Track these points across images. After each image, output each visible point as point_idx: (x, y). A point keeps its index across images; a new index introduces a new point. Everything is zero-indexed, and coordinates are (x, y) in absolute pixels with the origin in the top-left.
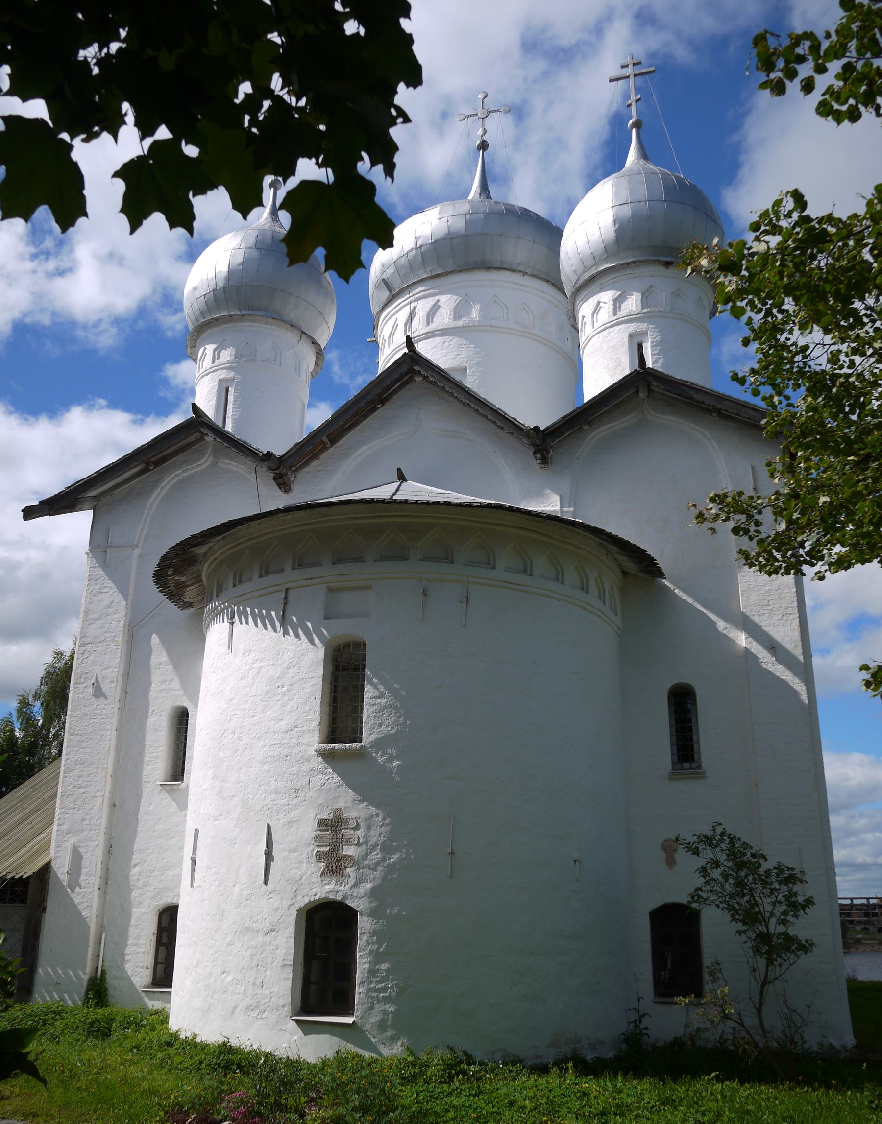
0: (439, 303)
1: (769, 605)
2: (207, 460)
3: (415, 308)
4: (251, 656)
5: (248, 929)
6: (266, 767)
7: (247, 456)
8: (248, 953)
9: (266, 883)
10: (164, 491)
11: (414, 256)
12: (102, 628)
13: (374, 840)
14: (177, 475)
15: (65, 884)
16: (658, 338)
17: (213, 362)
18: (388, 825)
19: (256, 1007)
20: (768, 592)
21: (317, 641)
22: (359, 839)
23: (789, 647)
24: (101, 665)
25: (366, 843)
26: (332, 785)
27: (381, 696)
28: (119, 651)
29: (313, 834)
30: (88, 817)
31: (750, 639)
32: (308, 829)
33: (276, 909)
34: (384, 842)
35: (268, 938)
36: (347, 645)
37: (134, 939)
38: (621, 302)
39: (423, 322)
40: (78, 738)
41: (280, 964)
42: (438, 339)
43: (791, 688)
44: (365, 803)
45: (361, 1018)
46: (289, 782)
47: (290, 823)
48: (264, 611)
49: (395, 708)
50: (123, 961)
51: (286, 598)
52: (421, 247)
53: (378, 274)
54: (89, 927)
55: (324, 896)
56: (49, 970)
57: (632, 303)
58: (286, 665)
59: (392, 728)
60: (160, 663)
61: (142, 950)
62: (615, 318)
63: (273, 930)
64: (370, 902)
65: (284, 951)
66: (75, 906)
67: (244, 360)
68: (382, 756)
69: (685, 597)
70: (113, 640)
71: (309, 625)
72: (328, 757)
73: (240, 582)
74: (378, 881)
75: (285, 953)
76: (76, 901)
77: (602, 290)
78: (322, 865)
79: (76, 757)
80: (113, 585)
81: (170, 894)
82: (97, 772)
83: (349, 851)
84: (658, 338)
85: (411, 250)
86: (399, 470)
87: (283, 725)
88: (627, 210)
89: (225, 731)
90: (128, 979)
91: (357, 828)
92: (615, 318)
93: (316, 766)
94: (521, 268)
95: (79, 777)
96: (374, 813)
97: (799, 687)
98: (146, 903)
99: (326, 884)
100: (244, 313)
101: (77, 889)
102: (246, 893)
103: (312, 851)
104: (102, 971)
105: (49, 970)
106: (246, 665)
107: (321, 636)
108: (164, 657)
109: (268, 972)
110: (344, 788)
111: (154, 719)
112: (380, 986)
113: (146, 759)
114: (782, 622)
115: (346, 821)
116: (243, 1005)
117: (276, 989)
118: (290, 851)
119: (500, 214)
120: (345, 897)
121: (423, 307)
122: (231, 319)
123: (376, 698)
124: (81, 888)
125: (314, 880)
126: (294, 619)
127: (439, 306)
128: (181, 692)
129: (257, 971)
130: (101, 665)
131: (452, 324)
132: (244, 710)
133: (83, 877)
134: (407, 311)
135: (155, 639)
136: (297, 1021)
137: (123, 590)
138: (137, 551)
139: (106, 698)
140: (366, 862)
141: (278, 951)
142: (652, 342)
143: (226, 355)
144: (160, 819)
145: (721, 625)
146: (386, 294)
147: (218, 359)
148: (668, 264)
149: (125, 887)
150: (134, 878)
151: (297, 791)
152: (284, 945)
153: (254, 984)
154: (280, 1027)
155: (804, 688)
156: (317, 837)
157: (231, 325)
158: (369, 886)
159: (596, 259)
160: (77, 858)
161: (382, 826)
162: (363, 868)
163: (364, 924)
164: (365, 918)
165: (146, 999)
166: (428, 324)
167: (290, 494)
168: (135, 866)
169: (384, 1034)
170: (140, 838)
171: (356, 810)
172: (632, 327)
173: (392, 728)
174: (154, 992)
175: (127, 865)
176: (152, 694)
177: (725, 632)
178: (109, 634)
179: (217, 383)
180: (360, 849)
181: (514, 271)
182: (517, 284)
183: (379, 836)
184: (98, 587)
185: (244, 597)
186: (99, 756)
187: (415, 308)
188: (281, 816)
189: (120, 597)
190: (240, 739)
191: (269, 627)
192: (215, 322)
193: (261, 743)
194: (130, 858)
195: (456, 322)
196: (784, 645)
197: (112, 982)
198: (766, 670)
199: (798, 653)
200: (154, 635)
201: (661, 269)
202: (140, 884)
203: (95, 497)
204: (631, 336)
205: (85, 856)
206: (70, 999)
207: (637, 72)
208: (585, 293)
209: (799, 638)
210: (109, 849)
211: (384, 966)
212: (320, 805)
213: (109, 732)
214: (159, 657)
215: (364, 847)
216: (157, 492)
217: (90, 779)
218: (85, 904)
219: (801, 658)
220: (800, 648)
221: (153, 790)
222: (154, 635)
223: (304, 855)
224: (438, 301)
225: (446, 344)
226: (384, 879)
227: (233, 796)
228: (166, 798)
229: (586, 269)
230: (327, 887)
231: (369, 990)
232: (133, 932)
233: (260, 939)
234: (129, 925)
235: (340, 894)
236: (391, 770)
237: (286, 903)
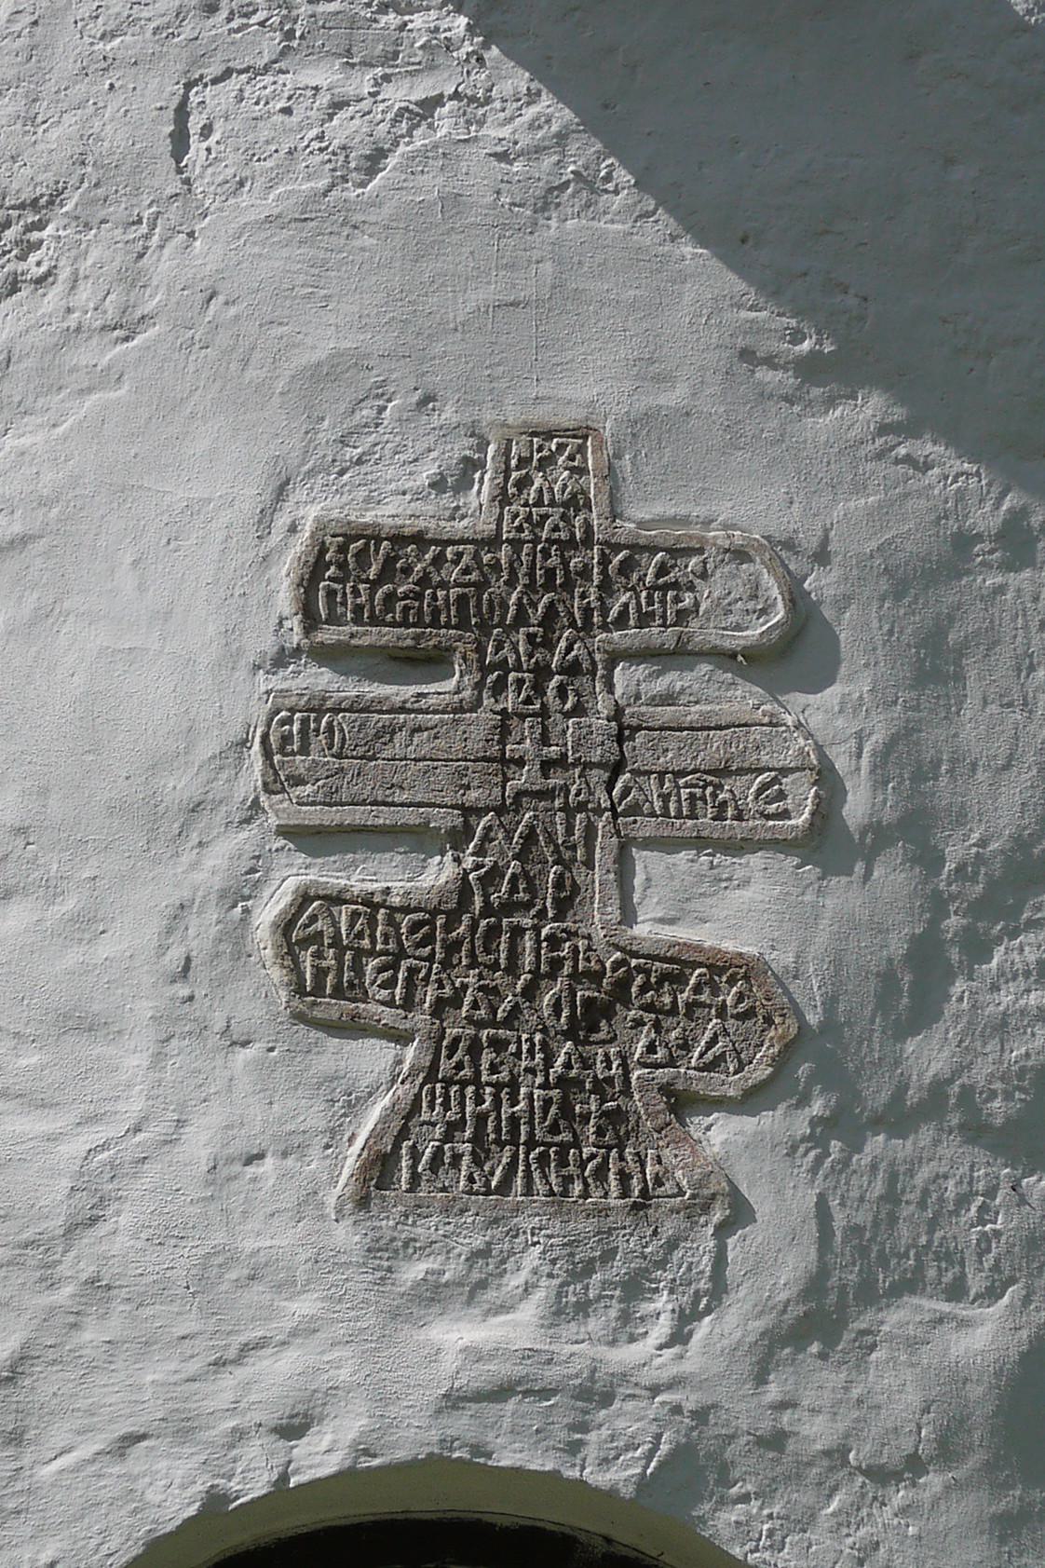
22: (826, 776)
25: (914, 831)
29: (249, 701)
44: (870, 407)
55: (413, 1436)
78: (377, 1067)
91: (797, 653)
99: (433, 1295)
103: (240, 894)
110: (620, 218)
120: (691, 1468)
140: (929, 1056)
156: (291, 739)
158: (985, 1335)
162: (897, 1120)
171: (768, 474)
180: (843, 896)
212: (322, 375)
215: (892, 876)
223: (130, 937)
230: (456, 1337)
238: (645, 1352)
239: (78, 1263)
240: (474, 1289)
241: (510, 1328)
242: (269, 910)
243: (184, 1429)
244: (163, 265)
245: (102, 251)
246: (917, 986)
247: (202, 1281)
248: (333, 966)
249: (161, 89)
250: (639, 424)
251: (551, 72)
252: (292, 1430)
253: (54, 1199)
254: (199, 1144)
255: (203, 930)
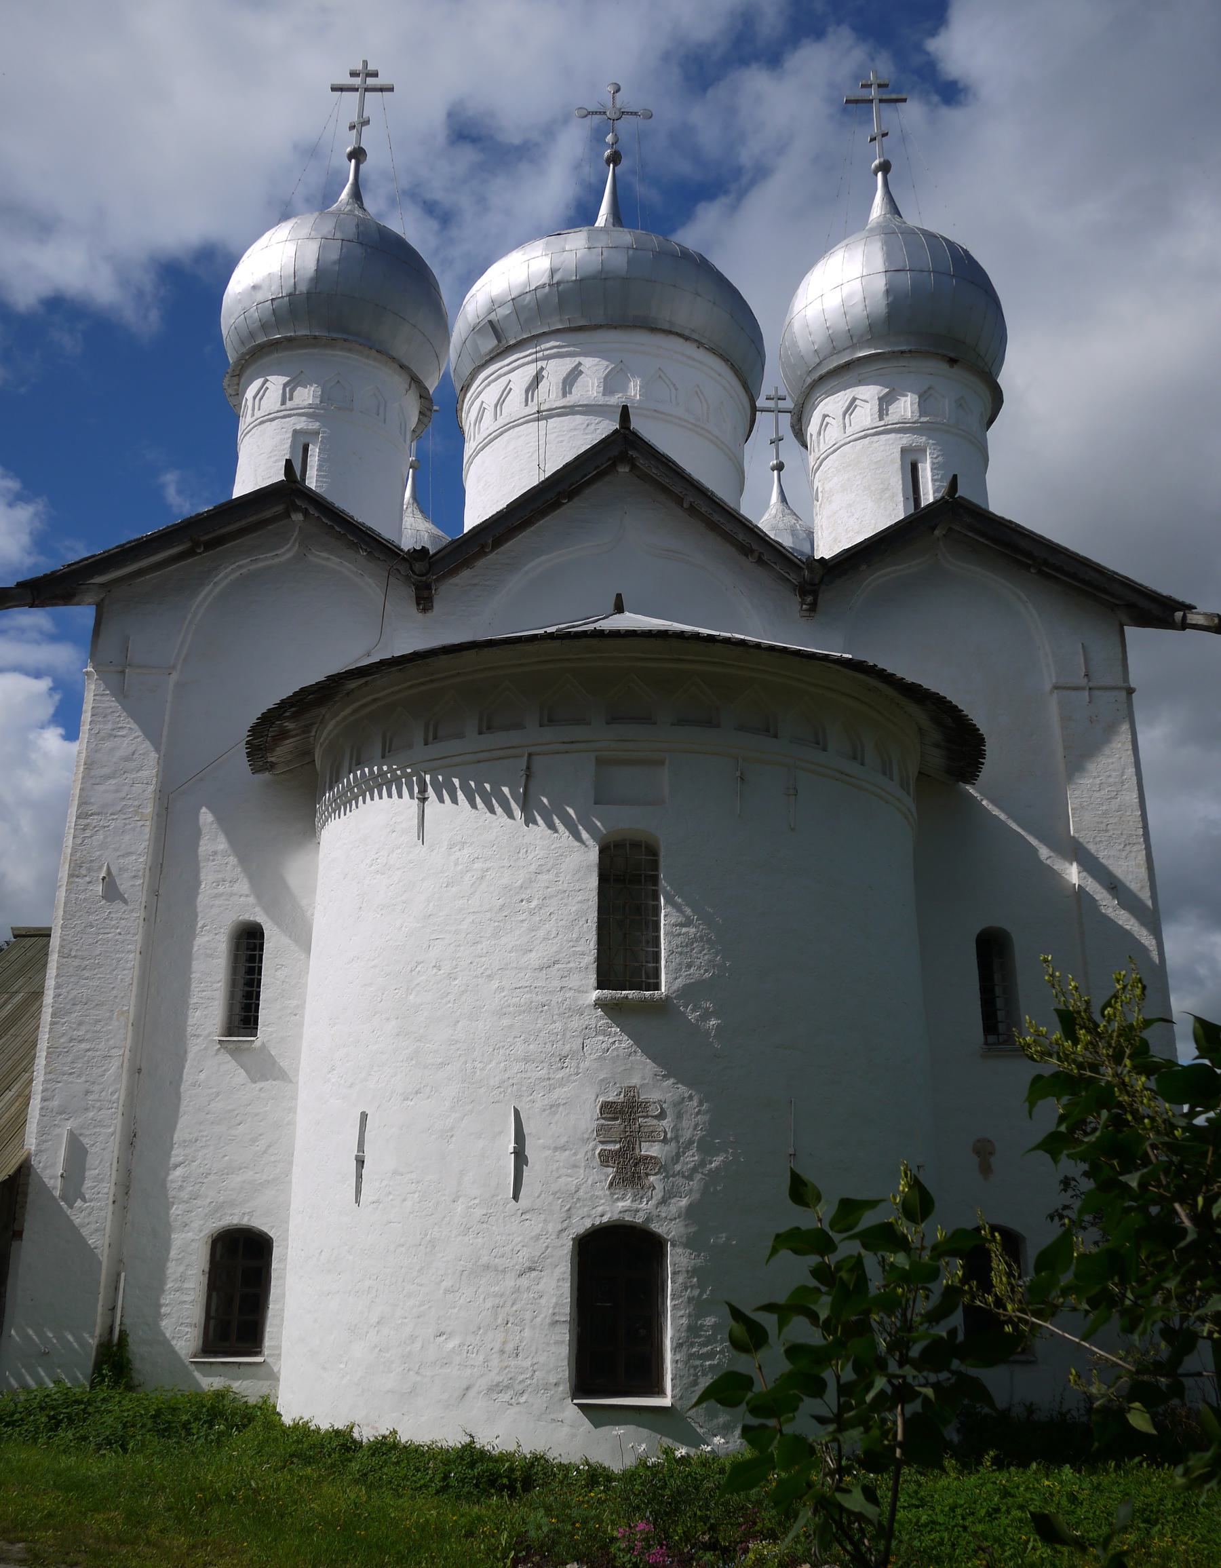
0: (581, 368)
1: (1107, 831)
2: (289, 550)
3: (542, 369)
4: (465, 851)
5: (487, 1267)
6: (506, 1022)
7: (354, 546)
8: (489, 1304)
9: (516, 1197)
10: (218, 589)
11: (547, 296)
12: (117, 791)
13: (687, 1135)
14: (240, 567)
15: (57, 1193)
16: (940, 459)
17: (283, 403)
18: (707, 1112)
19: (507, 1387)
20: (1105, 813)
21: (585, 835)
22: (665, 1132)
23: (1134, 886)
24: (116, 850)
25: (676, 1138)
26: (621, 1051)
27: (688, 923)
28: (147, 829)
29: (595, 1124)
30: (96, 1088)
31: (1085, 874)
32: (586, 1117)
33: (537, 1238)
34: (702, 1139)
35: (524, 1282)
36: (636, 845)
37: (175, 1280)
38: (890, 403)
39: (556, 391)
40: (77, 962)
41: (548, 1321)
42: (579, 419)
43: (1138, 942)
44: (672, 1080)
45: (681, 1398)
46: (548, 1045)
47: (553, 1107)
48: (487, 786)
49: (709, 941)
50: (158, 1316)
51: (528, 768)
52: (558, 283)
53: (482, 310)
54: (100, 1263)
55: (616, 1217)
56: (31, 1332)
57: (906, 407)
58: (533, 868)
59: (706, 971)
60: (215, 853)
61: (188, 1298)
62: (882, 423)
63: (531, 1269)
64: (686, 1226)
65: (554, 1300)
66: (74, 1229)
67: (332, 408)
68: (693, 1011)
69: (996, 812)
70: (136, 813)
71: (571, 811)
72: (610, 1009)
73: (435, 738)
74: (696, 1196)
75: (556, 1304)
76: (77, 1221)
77: (860, 383)
78: (611, 1171)
79: (74, 993)
80: (134, 726)
81: (236, 1211)
82: (110, 1018)
83: (651, 1150)
84: (940, 459)
85: (543, 286)
86: (619, 596)
87: (534, 958)
88: (906, 279)
89: (418, 963)
90: (166, 1344)
91: (662, 1116)
92: (882, 423)
93: (593, 1022)
94: (695, 336)
95: (80, 1024)
96: (686, 1095)
97: (1147, 940)
98: (196, 1225)
99: (618, 1199)
100: (335, 335)
101: (79, 1203)
102: (479, 1212)
103: (594, 1150)
104: (121, 1331)
105: (31, 1332)
106: (456, 864)
107: (591, 830)
108: (222, 844)
109: (527, 1333)
110: (639, 1057)
111: (206, 939)
112: (705, 1350)
113: (193, 1000)
114: (1124, 854)
115: (645, 1105)
116: (483, 1383)
117: (542, 1359)
118: (556, 1149)
119: (673, 255)
120: (649, 1219)
121: (556, 370)
122: (312, 342)
123: (682, 925)
124: (84, 1200)
125: (600, 1193)
126: (545, 800)
127: (581, 372)
128: (252, 900)
129: (507, 1332)
130: (116, 850)
131: (602, 400)
132: (457, 932)
133: (88, 1184)
134: (531, 370)
135: (206, 817)
136: (580, 1406)
137: (152, 735)
138: (175, 676)
139: (125, 902)
140: (678, 1167)
141: (543, 1301)
142: (933, 464)
143: (306, 396)
144: (218, 1094)
145: (1044, 852)
146: (490, 343)
147: (291, 399)
148: (952, 361)
149: (160, 1198)
150: (174, 1185)
151: (563, 1058)
152: (555, 1288)
153: (502, 1352)
154: (552, 1416)
155: (1154, 942)
156: (600, 1130)
157: (316, 351)
158: (684, 1202)
159: (854, 338)
160: (77, 1153)
161: (698, 1114)
162: (674, 1176)
163: (676, 1260)
164: (679, 1250)
165: (197, 1375)
166: (564, 395)
167: (429, 614)
168: (176, 1166)
169: (715, 1422)
170: (182, 1122)
171: (659, 1091)
172: (906, 439)
173: (706, 971)
174: (240, 1364)
175: (163, 1165)
176: (202, 899)
177: (1048, 862)
178: (130, 803)
179: (290, 435)
180: (667, 1147)
181: (687, 339)
182: (689, 357)
183: (695, 1128)
184: (109, 726)
185: (446, 761)
186: (115, 992)
187: (542, 369)
188: (537, 1096)
189: (147, 745)
190: (451, 976)
191: (499, 810)
192: (274, 345)
193: (495, 984)
194: (167, 1154)
195: (607, 398)
196: (1128, 884)
197: (136, 1348)
198: (1105, 916)
199: (1145, 895)
200: (204, 810)
201: (944, 367)
202: (184, 1195)
203: (102, 585)
204: (904, 451)
205: (93, 1150)
206: (50, 1377)
207: (885, 97)
208: (833, 383)
209: (1146, 877)
210: (131, 1140)
211: (710, 1321)
212: (602, 1080)
213: (131, 956)
214: (213, 843)
215: (673, 1144)
216: (208, 589)
217: (98, 1028)
218: (93, 1226)
219: (1149, 903)
220: (1148, 889)
221: (205, 1049)
222: (204, 810)
223: (580, 1156)
224: (580, 364)
225: (592, 427)
226: (705, 1192)
227: (443, 1065)
228: (227, 1063)
229: (835, 351)
230: (620, 1204)
231: (691, 1356)
232: (173, 1270)
233: (510, 1282)
234: (167, 1259)
235: (641, 1214)
236: (708, 1033)
237: (553, 1227)
238: (643, 1205)
239: (576, 1196)
240: (623, 1199)
241: (627, 1203)
242: (597, 1152)
243: (589, 1216)
244: (582, 1065)
245: (574, 1063)
246: (676, 1158)
247: (591, 1198)
248: (605, 1159)
249: (580, 1040)
250: (642, 1086)
251: (630, 1037)
252: (602, 1216)
253: (573, 1188)
254: (590, 1182)
255: (589, 1154)
